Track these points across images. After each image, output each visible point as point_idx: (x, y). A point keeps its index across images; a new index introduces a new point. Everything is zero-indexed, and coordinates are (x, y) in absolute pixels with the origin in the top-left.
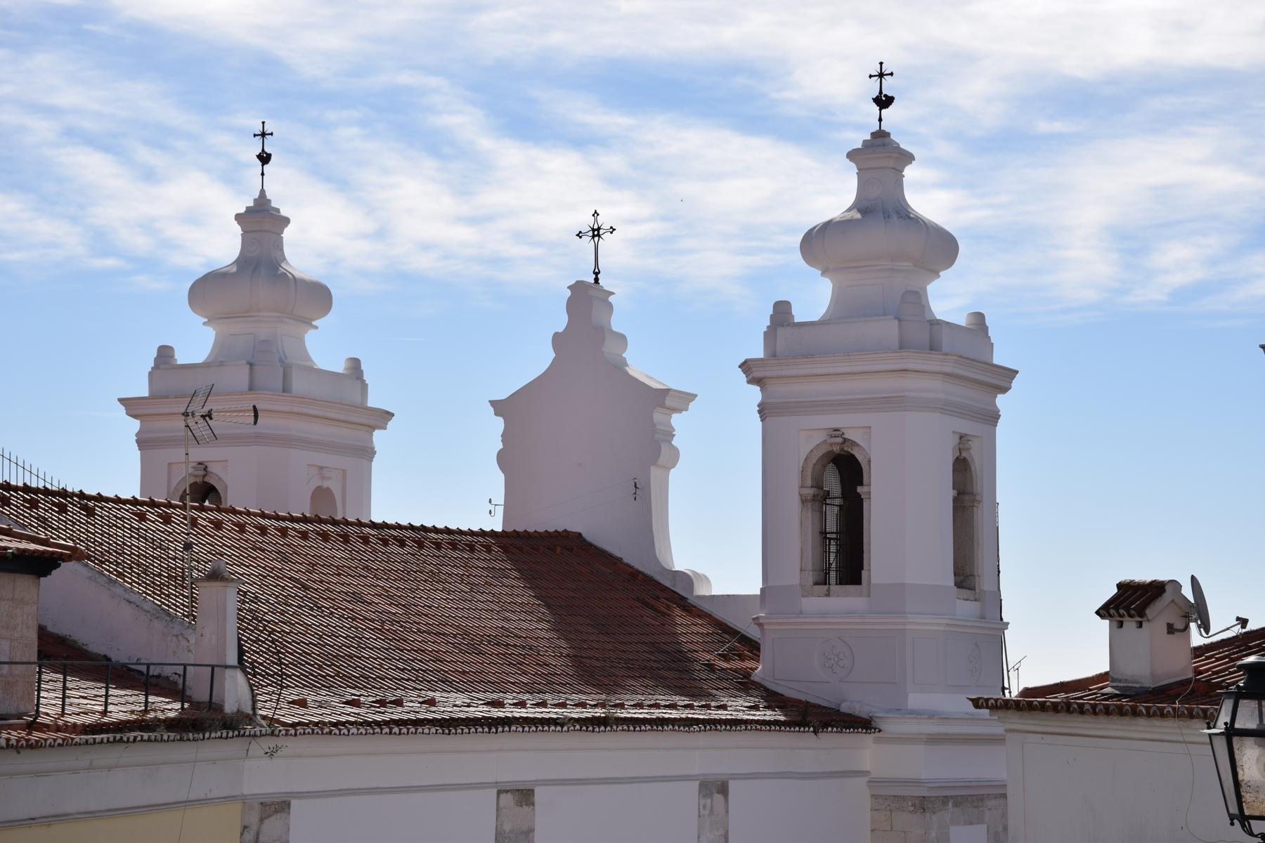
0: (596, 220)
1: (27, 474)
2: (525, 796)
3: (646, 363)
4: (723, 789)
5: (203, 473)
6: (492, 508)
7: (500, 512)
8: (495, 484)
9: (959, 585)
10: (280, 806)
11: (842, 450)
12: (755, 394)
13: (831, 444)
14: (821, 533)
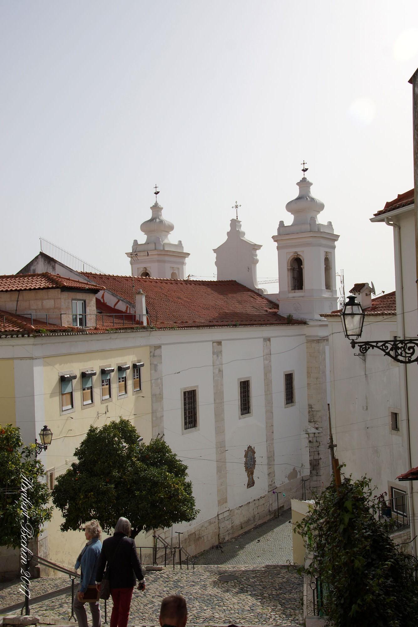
2: (219, 343)
3: (250, 237)
4: (269, 340)
7: (216, 276)
8: (215, 270)
9: (327, 288)
10: (159, 347)
12: (276, 244)
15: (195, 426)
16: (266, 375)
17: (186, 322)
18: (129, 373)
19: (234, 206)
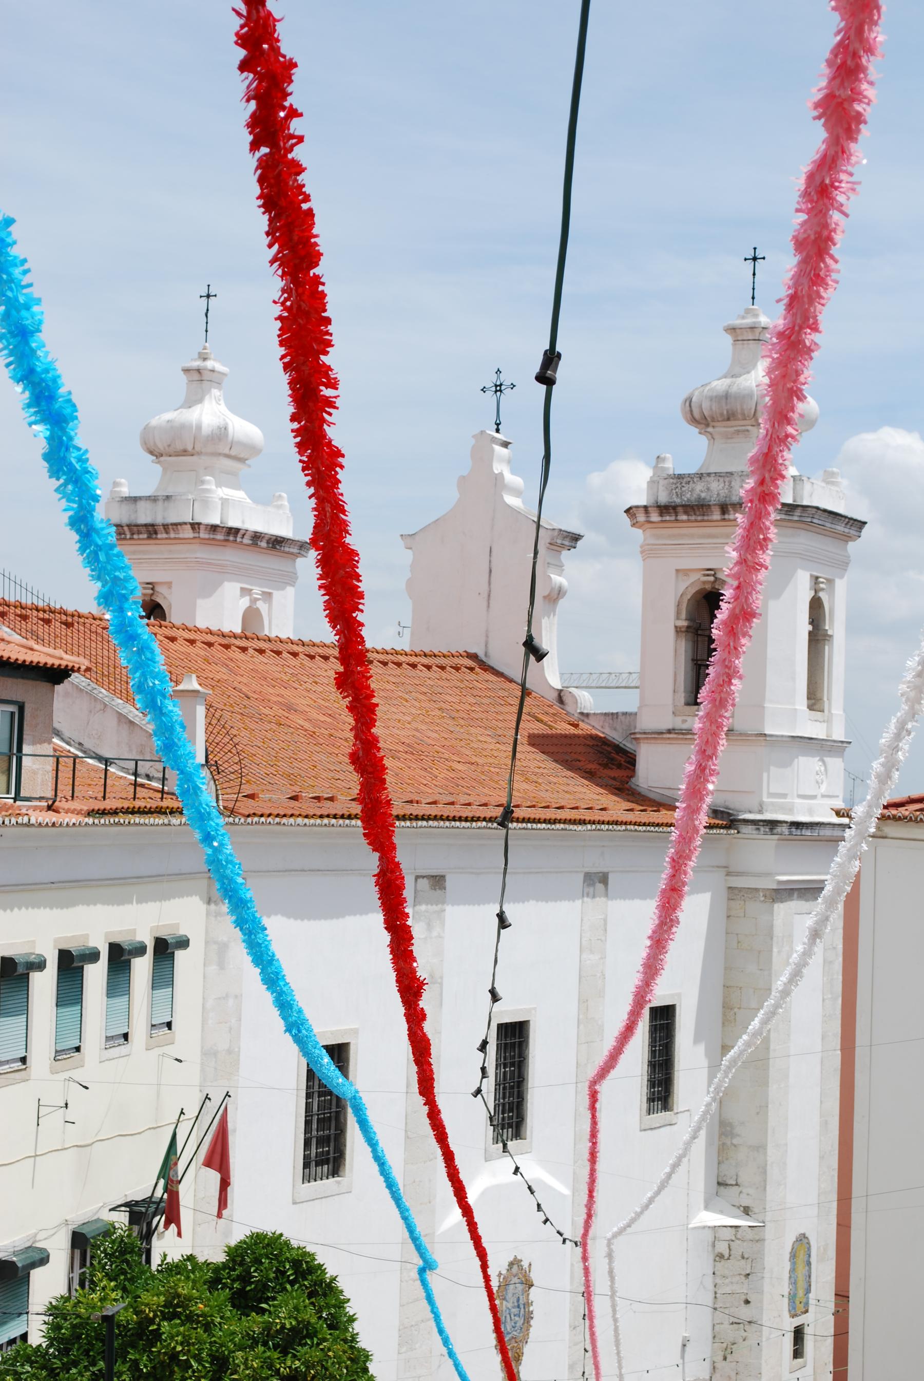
0: (498, 377)
1: (29, 594)
5: (151, 592)
6: (401, 629)
7: (407, 633)
9: (811, 708)
11: (714, 588)
13: (704, 583)
14: (693, 660)
15: (336, 1170)
16: (583, 1001)
17: (331, 799)
18: (142, 967)
19: (489, 384)
